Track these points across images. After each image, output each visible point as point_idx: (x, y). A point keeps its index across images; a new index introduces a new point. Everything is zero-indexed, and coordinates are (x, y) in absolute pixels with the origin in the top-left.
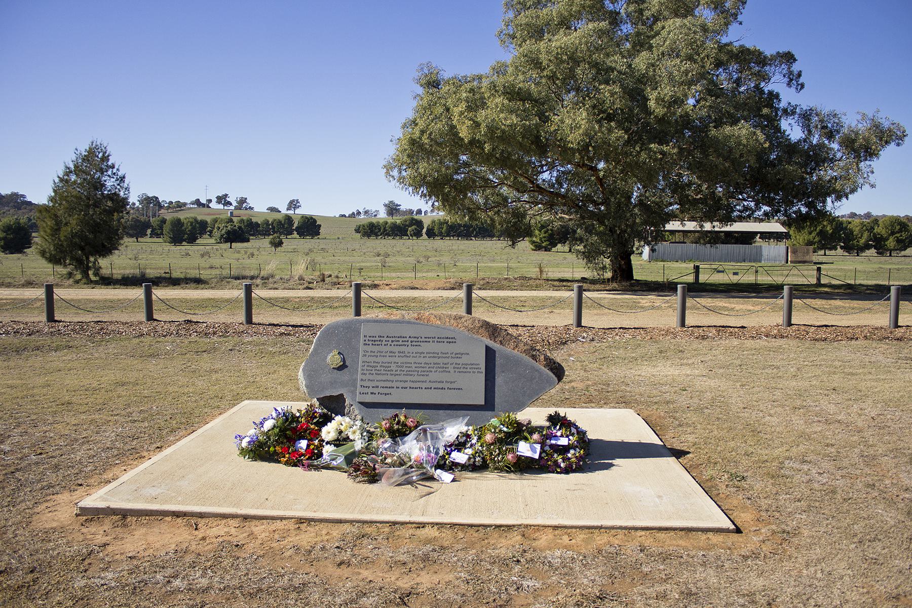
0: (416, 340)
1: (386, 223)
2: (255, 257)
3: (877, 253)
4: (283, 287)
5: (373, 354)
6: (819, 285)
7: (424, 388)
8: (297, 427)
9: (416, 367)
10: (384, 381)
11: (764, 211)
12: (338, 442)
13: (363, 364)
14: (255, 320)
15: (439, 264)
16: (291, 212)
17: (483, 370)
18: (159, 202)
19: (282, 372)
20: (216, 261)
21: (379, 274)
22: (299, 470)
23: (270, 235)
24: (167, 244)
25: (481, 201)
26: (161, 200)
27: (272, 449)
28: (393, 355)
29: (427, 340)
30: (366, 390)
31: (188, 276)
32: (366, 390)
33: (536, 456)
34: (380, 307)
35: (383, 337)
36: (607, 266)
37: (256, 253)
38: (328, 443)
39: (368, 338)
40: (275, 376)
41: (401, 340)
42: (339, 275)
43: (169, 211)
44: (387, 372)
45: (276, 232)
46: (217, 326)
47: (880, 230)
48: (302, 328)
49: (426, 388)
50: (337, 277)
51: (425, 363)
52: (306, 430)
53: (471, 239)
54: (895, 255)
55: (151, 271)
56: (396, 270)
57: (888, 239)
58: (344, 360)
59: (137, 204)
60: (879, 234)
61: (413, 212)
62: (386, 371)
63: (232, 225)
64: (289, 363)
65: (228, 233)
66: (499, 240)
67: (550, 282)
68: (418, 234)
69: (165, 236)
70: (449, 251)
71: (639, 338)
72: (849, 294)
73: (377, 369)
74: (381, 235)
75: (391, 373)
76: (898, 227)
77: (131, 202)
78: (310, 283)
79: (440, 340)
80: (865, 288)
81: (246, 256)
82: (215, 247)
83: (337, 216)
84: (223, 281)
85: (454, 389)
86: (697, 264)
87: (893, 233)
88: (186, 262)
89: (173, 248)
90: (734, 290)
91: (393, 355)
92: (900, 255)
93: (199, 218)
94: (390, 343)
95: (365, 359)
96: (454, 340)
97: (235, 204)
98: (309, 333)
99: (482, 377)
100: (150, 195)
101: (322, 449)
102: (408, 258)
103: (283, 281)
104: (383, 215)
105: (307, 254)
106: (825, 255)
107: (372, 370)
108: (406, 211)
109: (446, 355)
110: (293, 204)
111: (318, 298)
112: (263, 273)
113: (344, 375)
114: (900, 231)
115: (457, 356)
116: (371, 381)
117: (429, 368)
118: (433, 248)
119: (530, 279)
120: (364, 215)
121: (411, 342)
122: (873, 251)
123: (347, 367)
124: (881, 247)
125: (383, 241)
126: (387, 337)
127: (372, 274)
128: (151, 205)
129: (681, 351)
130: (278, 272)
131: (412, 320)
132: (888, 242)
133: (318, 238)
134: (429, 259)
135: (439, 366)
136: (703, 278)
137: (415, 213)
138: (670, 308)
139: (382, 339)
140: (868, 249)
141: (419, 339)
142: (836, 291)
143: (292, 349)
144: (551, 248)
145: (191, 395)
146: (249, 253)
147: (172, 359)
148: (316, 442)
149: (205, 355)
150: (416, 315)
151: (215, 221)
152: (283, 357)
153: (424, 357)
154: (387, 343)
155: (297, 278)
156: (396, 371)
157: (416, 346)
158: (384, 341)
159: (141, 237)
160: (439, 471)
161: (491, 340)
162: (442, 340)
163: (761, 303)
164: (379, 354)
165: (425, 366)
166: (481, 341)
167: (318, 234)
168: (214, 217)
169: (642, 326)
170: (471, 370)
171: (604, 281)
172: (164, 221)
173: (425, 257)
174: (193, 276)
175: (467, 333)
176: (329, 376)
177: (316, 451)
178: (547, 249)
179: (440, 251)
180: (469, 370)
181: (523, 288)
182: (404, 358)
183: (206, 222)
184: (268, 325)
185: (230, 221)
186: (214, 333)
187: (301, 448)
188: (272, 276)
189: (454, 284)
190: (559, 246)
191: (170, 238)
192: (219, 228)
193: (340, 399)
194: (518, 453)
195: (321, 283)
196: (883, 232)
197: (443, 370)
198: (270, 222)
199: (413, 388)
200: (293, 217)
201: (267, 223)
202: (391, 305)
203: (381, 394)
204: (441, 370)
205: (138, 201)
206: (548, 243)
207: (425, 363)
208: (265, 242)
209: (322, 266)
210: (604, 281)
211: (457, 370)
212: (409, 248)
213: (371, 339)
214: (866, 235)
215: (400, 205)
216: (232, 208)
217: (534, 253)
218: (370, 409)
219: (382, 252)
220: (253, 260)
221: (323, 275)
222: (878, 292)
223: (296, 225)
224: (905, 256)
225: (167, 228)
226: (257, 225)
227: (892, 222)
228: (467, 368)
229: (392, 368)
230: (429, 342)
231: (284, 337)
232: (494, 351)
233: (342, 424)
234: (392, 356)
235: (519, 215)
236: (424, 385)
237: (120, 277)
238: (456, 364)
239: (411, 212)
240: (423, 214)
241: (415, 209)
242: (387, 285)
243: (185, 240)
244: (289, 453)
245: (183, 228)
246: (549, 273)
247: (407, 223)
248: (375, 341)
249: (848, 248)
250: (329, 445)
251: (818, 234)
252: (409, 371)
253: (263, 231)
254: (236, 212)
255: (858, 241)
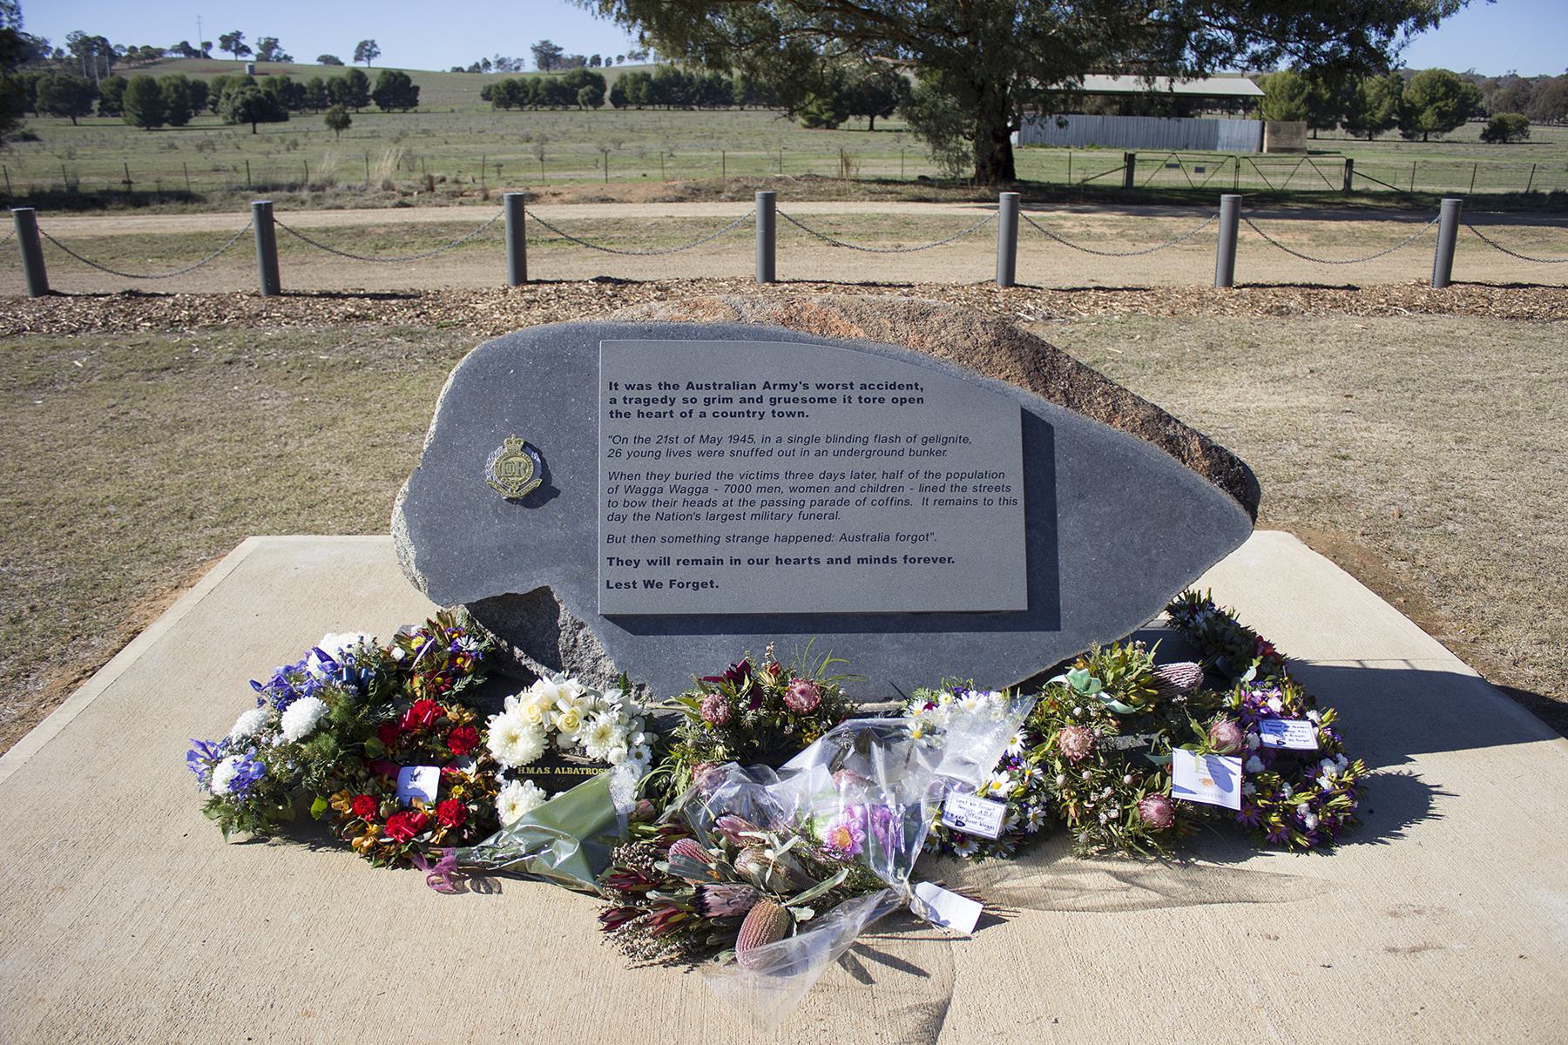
0: (787, 393)
1: (538, 81)
2: (301, 147)
3: (1403, 135)
4: (353, 204)
5: (643, 448)
6: (1348, 191)
7: (823, 560)
8: (399, 718)
9: (793, 490)
10: (688, 540)
11: (1253, 52)
12: (547, 770)
13: (613, 484)
14: (286, 284)
15: (642, 155)
16: (362, 65)
17: (1018, 492)
18: (108, 47)
19: (352, 421)
20: (227, 158)
21: (539, 175)
22: (417, 878)
23: (325, 107)
24: (134, 128)
25: (731, 29)
26: (112, 44)
27: (318, 806)
28: (713, 447)
29: (827, 393)
30: (627, 574)
31: (166, 187)
32: (627, 574)
33: (1234, 801)
34: (551, 241)
35: (676, 387)
36: (971, 155)
37: (301, 140)
38: (511, 774)
39: (622, 392)
40: (332, 436)
41: (736, 394)
42: (461, 178)
43: (132, 65)
44: (697, 510)
45: (338, 102)
46: (197, 302)
47: (1410, 93)
48: (394, 302)
49: (830, 561)
50: (457, 182)
51: (823, 475)
52: (431, 730)
53: (692, 109)
54: (1435, 139)
55: (94, 179)
56: (566, 166)
57: (1422, 111)
58: (544, 471)
59: (67, 52)
60: (1409, 102)
61: (586, 60)
62: (692, 504)
63: (253, 90)
64: (367, 396)
65: (247, 104)
66: (742, 109)
67: (863, 185)
68: (596, 101)
69: (127, 113)
70: (656, 130)
71: (1145, 311)
72: (1406, 211)
73: (662, 497)
74: (529, 103)
75: (712, 510)
76: (1442, 90)
77: (55, 48)
78: (405, 194)
79: (871, 392)
80: (1432, 199)
81: (282, 148)
82: (224, 132)
83: (448, 70)
84: (231, 197)
85: (926, 560)
86: (1129, 152)
87: (1432, 101)
88: (168, 161)
89: (144, 135)
90: (1201, 200)
91: (713, 447)
92: (1440, 140)
93: (191, 78)
94: (699, 407)
95: (620, 465)
96: (915, 394)
97: (256, 50)
98: (412, 313)
99: (1017, 515)
100: (91, 34)
101: (493, 798)
102: (583, 145)
103: (353, 191)
104: (530, 67)
105: (397, 141)
106: (1315, 138)
107: (643, 504)
108: (573, 59)
109: (892, 446)
110: (366, 50)
111: (426, 224)
112: (313, 178)
113: (549, 524)
114: (1446, 96)
115: (929, 446)
116: (644, 540)
117: (838, 489)
118: (625, 124)
119: (825, 178)
120: (498, 67)
121: (773, 401)
122: (1396, 132)
123: (555, 493)
124: (1411, 126)
125: (534, 115)
126: (690, 386)
127: (522, 175)
128: (96, 54)
129: (1252, 345)
130: (344, 175)
131: (771, 327)
132: (1424, 116)
133: (416, 112)
134: (623, 146)
135: (871, 482)
136: (1141, 177)
137: (588, 62)
138: (1123, 236)
139: (670, 393)
140: (1389, 128)
141: (800, 392)
142: (1383, 204)
143: (374, 355)
144: (837, 124)
145: (112, 509)
146: (288, 142)
147: (83, 393)
148: (471, 771)
149: (167, 378)
150: (779, 307)
151: (222, 82)
152: (352, 377)
153: (818, 454)
154: (690, 406)
155: (379, 185)
156: (726, 504)
157: (791, 414)
158: (679, 401)
159: (82, 115)
160: (925, 889)
161: (1035, 390)
162: (877, 394)
163: (1288, 229)
164: (663, 448)
165: (825, 483)
166: (1005, 394)
167: (415, 103)
168: (219, 75)
169: (1145, 284)
170: (980, 496)
171: (964, 184)
172: (122, 84)
173: (613, 141)
174: (173, 188)
175: (955, 367)
176: (497, 526)
177: (473, 807)
178: (830, 126)
179: (640, 130)
180: (970, 495)
181: (814, 197)
182: (753, 459)
183: (204, 86)
184: (317, 296)
185: (250, 81)
186: (193, 321)
187: (421, 796)
188: (332, 184)
189: (683, 192)
190: (852, 120)
191: (138, 115)
192: (230, 96)
193: (541, 603)
194: (1174, 795)
195: (427, 195)
196: (1417, 98)
197: (884, 496)
198: (325, 84)
199: (787, 561)
200: (367, 73)
201: (318, 84)
202: (573, 237)
203: (681, 585)
204: (879, 496)
205: (69, 45)
206: (831, 114)
207: (823, 475)
208: (317, 121)
209: (427, 162)
210: (964, 184)
211: (932, 496)
212: (582, 126)
213: (634, 394)
214: (1387, 103)
215: (561, 49)
216: (251, 58)
217: (808, 133)
218: (646, 638)
219: (534, 135)
220: (296, 155)
221: (431, 178)
222: (1415, 207)
223: (372, 88)
224: (1449, 142)
225: (129, 97)
226: (300, 88)
227: (1432, 80)
228: (964, 489)
229: (711, 495)
230: (833, 400)
231: (353, 324)
232: (1049, 428)
233: (555, 708)
234: (709, 453)
235: (803, 57)
236: (823, 551)
237: (25, 192)
238: (928, 474)
239: (581, 60)
240: (603, 65)
241: (589, 55)
242: (554, 195)
243: (166, 120)
244: (379, 820)
245: (161, 97)
246: (861, 169)
247: (576, 81)
248: (647, 402)
249: (1354, 127)
250: (516, 782)
251: (1305, 101)
252: (772, 503)
253: (312, 100)
254: (261, 66)
255: (1372, 115)
